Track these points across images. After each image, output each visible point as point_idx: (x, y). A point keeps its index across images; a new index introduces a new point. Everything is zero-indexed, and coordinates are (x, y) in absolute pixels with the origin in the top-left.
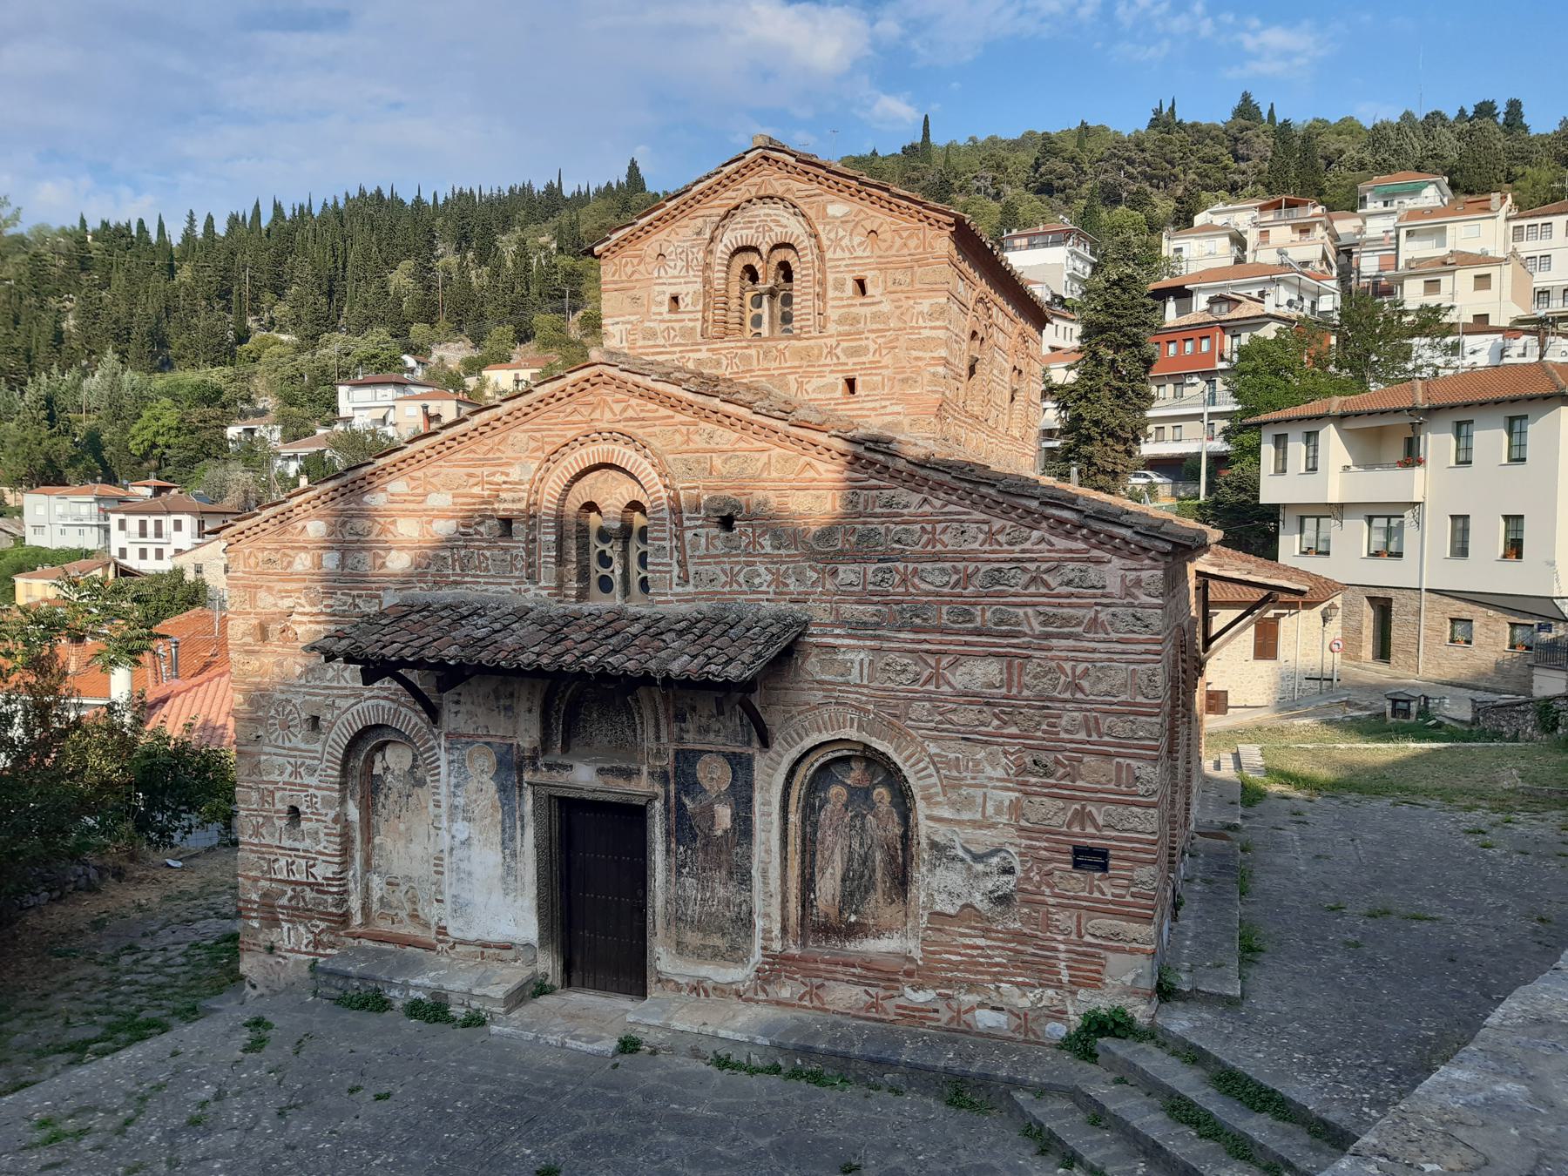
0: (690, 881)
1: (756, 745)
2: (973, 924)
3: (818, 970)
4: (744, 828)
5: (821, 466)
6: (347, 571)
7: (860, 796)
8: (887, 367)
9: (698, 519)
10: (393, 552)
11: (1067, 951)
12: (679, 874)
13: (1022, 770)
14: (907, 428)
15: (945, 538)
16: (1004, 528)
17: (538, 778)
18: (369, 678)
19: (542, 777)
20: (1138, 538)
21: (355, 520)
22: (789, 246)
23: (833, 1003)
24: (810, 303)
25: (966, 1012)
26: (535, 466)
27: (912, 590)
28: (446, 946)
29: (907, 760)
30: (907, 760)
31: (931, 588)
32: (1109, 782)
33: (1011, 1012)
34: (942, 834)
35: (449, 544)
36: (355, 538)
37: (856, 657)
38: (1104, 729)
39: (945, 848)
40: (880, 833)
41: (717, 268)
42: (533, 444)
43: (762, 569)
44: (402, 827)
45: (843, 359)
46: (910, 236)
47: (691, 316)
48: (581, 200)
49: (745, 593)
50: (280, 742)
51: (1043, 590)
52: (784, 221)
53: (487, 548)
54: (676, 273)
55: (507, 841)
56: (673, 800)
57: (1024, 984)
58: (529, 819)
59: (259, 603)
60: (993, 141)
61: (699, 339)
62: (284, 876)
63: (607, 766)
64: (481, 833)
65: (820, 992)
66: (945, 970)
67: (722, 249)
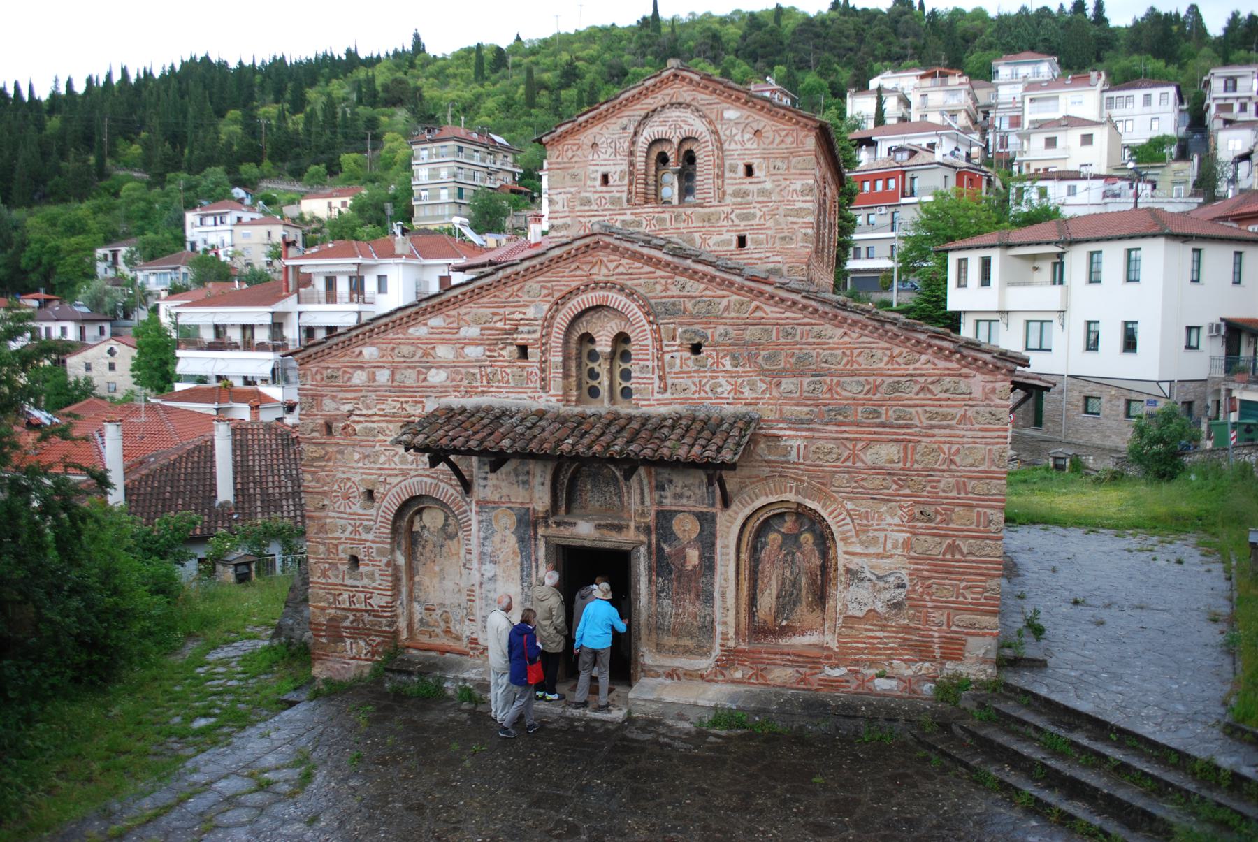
0: (666, 602)
1: (719, 505)
4: (708, 564)
6: (395, 384)
7: (792, 540)
8: (769, 228)
10: (433, 371)
12: (658, 597)
13: (913, 518)
14: (785, 273)
15: (860, 359)
16: (901, 353)
17: (550, 532)
18: (433, 463)
26: (546, 307)
28: (477, 652)
29: (830, 514)
30: (830, 514)
34: (855, 563)
37: (795, 443)
38: (970, 489)
39: (857, 572)
40: (806, 564)
42: (544, 292)
43: (723, 381)
44: (437, 569)
45: (737, 222)
46: (787, 135)
48: (372, 62)
50: (342, 509)
51: (929, 396)
52: (691, 121)
56: (654, 546)
57: (909, 660)
60: (709, 16)
61: (625, 205)
62: (347, 605)
63: (603, 523)
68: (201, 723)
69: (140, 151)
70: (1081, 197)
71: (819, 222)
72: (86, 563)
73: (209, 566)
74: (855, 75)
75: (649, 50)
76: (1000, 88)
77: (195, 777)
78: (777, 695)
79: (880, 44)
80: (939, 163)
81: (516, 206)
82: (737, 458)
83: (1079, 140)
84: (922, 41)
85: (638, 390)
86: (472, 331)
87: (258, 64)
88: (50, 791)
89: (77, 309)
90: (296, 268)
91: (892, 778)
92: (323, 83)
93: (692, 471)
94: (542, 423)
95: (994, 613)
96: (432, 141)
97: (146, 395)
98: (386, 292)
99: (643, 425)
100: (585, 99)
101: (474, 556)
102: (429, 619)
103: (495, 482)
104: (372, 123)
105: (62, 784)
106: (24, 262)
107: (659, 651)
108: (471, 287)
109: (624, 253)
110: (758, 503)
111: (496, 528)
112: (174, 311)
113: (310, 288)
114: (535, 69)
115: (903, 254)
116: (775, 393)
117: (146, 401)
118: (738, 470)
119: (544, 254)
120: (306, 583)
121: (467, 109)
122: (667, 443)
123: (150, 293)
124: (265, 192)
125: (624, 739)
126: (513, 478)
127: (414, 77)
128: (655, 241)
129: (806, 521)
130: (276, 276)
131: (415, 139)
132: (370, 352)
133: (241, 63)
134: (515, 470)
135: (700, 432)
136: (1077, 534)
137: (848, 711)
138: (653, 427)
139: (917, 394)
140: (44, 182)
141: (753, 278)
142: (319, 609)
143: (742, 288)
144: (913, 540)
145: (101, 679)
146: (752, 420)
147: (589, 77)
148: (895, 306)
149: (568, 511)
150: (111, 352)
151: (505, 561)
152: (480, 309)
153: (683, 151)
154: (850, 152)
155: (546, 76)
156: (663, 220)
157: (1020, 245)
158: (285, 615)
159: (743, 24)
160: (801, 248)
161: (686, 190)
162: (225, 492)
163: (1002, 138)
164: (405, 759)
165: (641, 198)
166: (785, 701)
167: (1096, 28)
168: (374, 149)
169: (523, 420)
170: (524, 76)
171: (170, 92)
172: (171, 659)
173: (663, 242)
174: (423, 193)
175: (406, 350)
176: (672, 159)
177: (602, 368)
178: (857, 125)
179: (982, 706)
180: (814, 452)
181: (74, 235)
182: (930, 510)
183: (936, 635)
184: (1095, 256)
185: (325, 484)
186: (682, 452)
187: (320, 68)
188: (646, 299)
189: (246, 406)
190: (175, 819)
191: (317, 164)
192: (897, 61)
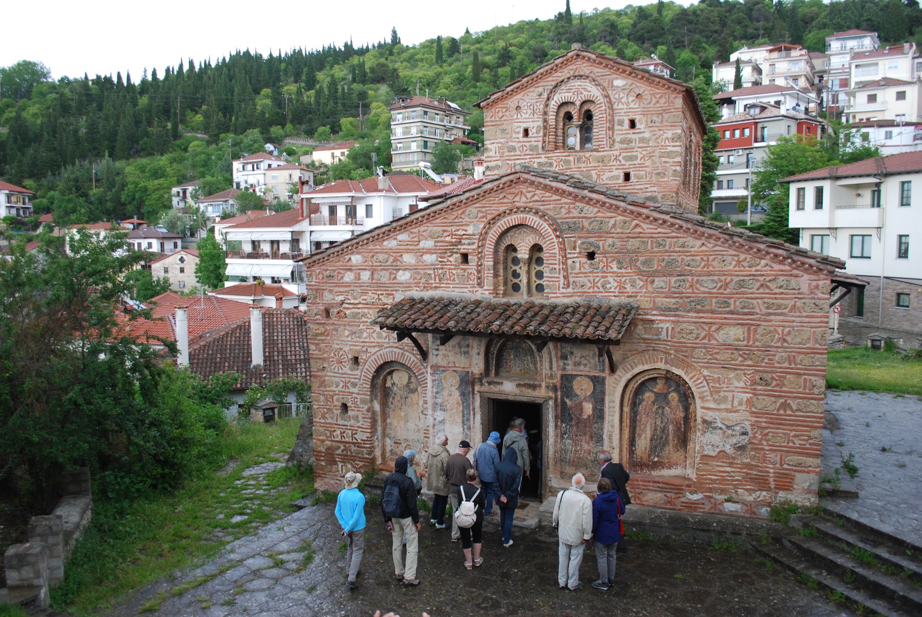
0: (568, 442)
1: (607, 371)
2: (725, 460)
3: (639, 485)
4: (599, 414)
5: (645, 226)
6: (374, 281)
7: (662, 398)
9: (574, 253)
10: (401, 272)
11: (774, 473)
12: (562, 438)
13: (754, 383)
14: (660, 199)
15: (714, 263)
17: (483, 389)
18: (400, 338)
19: (486, 388)
20: (819, 264)
21: (379, 255)
22: (592, 102)
23: (647, 501)
24: (604, 132)
25: (719, 504)
26: (482, 226)
27: (696, 291)
29: (691, 378)
30: (691, 378)
31: (707, 290)
32: (800, 388)
33: (743, 503)
34: (709, 416)
35: (432, 267)
36: (379, 264)
37: (665, 325)
38: (798, 361)
39: (711, 422)
40: (672, 416)
41: (551, 113)
43: (611, 280)
44: (403, 414)
45: (623, 162)
46: (661, 97)
47: (536, 139)
48: (362, 52)
49: (602, 292)
50: (336, 370)
51: (767, 291)
52: (589, 89)
53: (454, 269)
54: (527, 116)
55: (465, 421)
56: (559, 400)
57: (750, 489)
58: (478, 410)
59: (324, 298)
60: (607, 10)
61: (540, 151)
62: (339, 439)
63: (522, 383)
64: (450, 417)
65: (640, 496)
66: (709, 484)
67: (553, 104)
68: (238, 519)
69: (202, 119)
70: (895, 140)
71: (686, 161)
72: (162, 405)
73: (246, 410)
74: (719, 51)
75: (563, 37)
76: (831, 57)
77: (232, 556)
78: (650, 512)
79: (738, 27)
80: (783, 116)
81: (465, 153)
82: (620, 336)
83: (865, 99)
84: (771, 24)
85: (549, 286)
86: (428, 244)
87: (283, 55)
88: (135, 562)
89: (159, 230)
90: (309, 200)
91: (735, 577)
92: (328, 68)
93: (588, 346)
94: (478, 310)
95: (816, 456)
96: (405, 107)
97: (205, 290)
98: (372, 217)
99: (552, 311)
100: (516, 74)
101: (429, 405)
102: (397, 450)
103: (444, 352)
104: (363, 95)
105: (142, 557)
106: (123, 198)
107: (562, 478)
108: (428, 211)
109: (538, 186)
110: (637, 370)
111: (445, 385)
112: (224, 231)
113: (319, 214)
114: (480, 54)
115: (755, 185)
116: (650, 289)
117: (205, 294)
118: (622, 345)
119: (480, 187)
120: (311, 422)
121: (430, 84)
122: (569, 325)
123: (208, 219)
124: (287, 146)
125: (536, 540)
126: (457, 349)
127: (392, 61)
128: (561, 177)
129: (673, 383)
130: (295, 205)
131: (393, 107)
132: (356, 259)
133: (271, 55)
134: (459, 344)
135: (593, 317)
136: (887, 398)
137: (703, 526)
138: (558, 313)
139: (758, 289)
140: (137, 142)
141: (634, 204)
142: (320, 443)
143: (625, 211)
144: (755, 399)
145: (171, 486)
146: (632, 308)
147: (519, 58)
148: (749, 224)
149: (497, 374)
150: (182, 260)
151: (452, 409)
152: (434, 227)
153: (583, 111)
154: (714, 109)
155: (488, 59)
156: (568, 162)
157: (846, 177)
158: (297, 445)
159: (634, 15)
160: (672, 181)
161: (586, 139)
162: (257, 358)
163: (833, 96)
164: (377, 549)
165: (552, 146)
166: (656, 517)
167: (909, 9)
168: (364, 114)
169: (464, 307)
170: (471, 59)
171: (223, 77)
172: (219, 474)
173: (567, 178)
174: (399, 145)
175: (381, 257)
176: (575, 116)
177: (522, 270)
178: (720, 89)
179: (806, 525)
180: (679, 333)
181: (157, 178)
182: (767, 376)
183: (772, 471)
184: (906, 185)
185: (324, 353)
186: (579, 332)
187: (326, 58)
188: (554, 220)
189: (273, 298)
190: (218, 584)
191: (324, 126)
192: (751, 40)
